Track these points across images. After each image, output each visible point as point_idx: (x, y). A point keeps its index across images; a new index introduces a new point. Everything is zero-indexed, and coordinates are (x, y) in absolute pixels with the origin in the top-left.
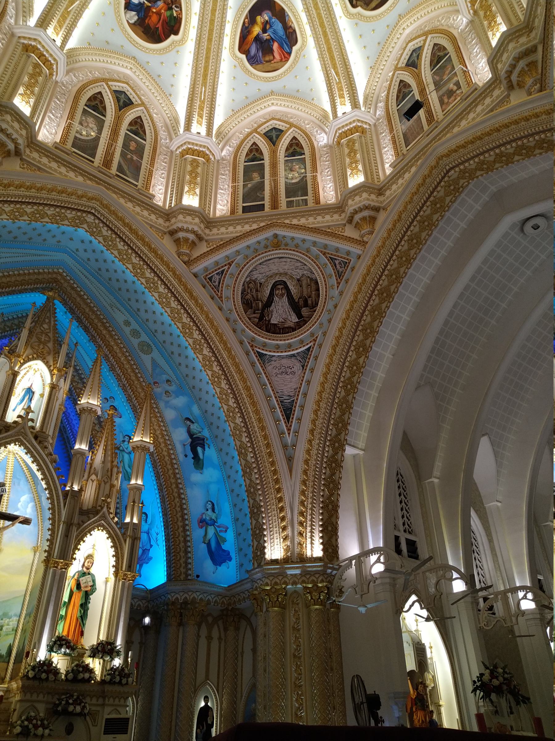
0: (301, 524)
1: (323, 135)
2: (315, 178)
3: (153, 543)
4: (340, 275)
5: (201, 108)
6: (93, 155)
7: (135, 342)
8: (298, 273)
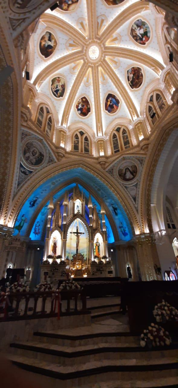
0: (143, 225)
1: (131, 126)
2: (131, 139)
3: (110, 233)
4: (141, 163)
5: (100, 129)
6: (78, 150)
7: (96, 189)
8: (131, 165)
